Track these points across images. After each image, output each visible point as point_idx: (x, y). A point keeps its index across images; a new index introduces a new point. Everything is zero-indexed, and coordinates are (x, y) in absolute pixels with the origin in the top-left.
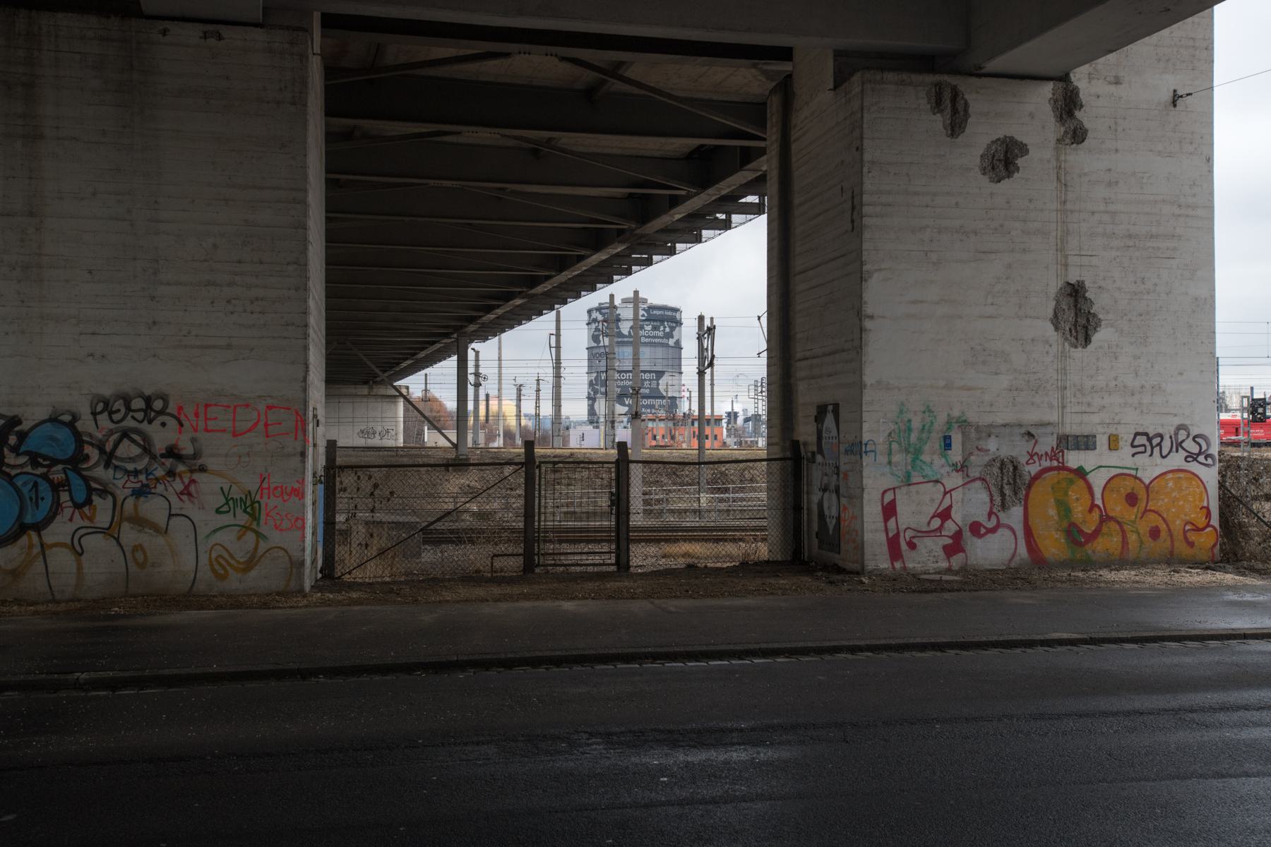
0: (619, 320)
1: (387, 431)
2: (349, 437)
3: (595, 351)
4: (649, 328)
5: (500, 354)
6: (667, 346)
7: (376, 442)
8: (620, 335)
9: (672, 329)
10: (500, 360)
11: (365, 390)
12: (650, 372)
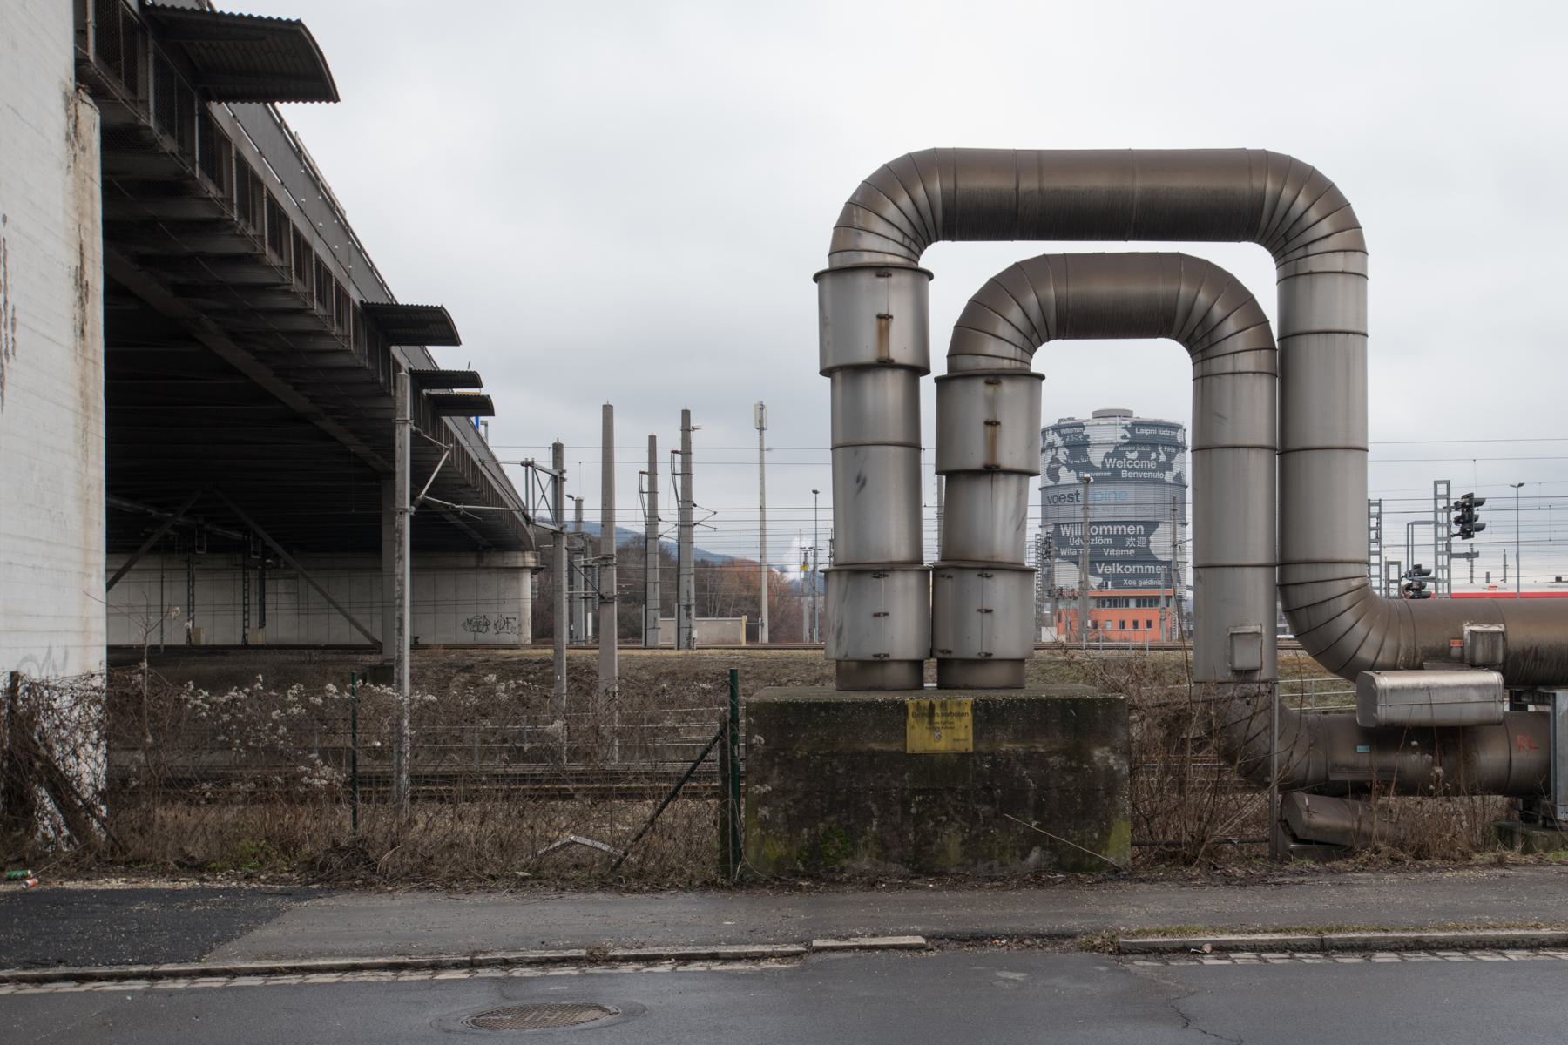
0: (1087, 445)
1: (507, 621)
2: (449, 630)
3: (1051, 493)
4: (1134, 455)
5: (762, 501)
6: (1162, 482)
7: (490, 636)
8: (1089, 467)
9: (1170, 457)
10: (762, 508)
11: (472, 561)
12: (1135, 523)
